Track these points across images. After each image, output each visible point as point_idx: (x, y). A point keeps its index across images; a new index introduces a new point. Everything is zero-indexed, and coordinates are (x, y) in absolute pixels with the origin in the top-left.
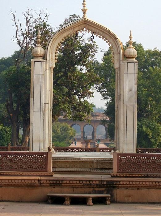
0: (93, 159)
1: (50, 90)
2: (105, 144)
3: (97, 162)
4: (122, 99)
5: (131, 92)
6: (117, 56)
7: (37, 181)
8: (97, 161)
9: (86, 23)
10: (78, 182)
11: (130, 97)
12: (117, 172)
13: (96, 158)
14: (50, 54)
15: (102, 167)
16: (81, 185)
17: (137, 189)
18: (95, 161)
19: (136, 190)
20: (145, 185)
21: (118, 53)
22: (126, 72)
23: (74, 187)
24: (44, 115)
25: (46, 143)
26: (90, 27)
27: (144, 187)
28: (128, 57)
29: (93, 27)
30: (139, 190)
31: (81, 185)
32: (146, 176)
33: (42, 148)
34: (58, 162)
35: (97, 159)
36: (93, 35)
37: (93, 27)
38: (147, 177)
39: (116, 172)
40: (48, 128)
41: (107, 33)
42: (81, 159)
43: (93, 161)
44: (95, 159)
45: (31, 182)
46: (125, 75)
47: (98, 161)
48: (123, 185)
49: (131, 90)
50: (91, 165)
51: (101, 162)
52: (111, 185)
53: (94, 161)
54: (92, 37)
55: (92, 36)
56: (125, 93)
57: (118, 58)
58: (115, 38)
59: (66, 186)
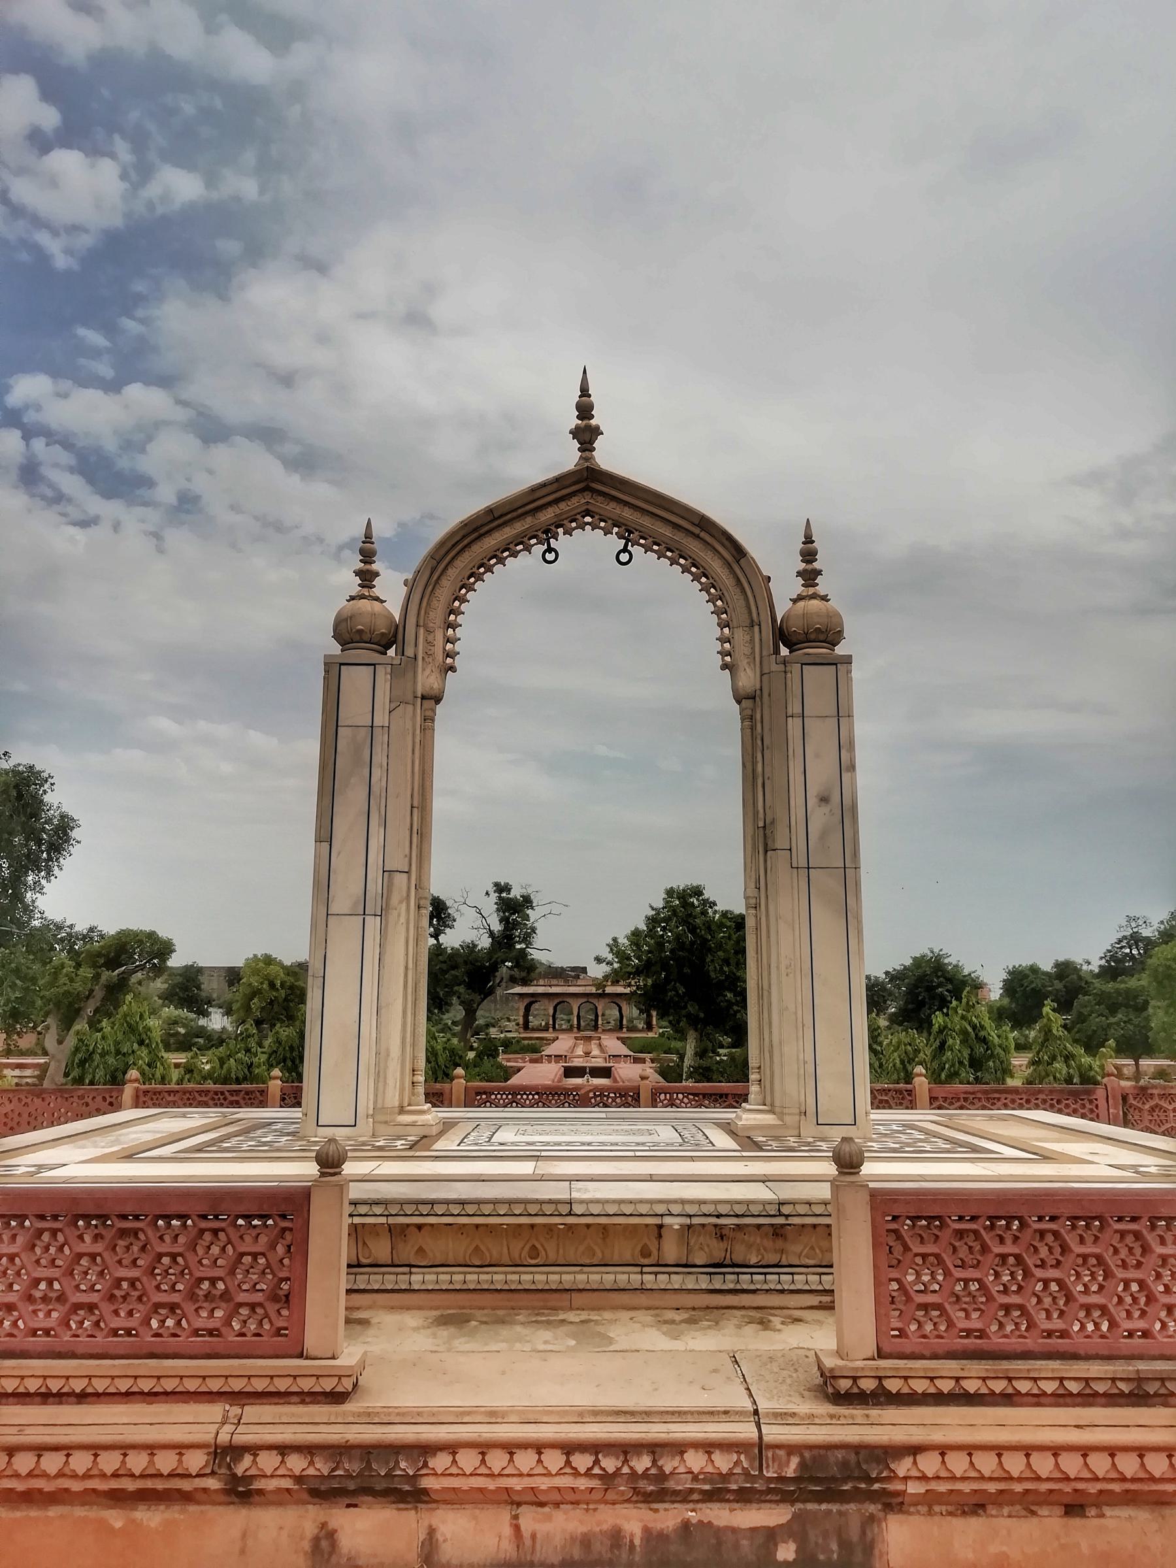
0: (660, 1209)
1: (415, 804)
2: (623, 1041)
3: (690, 1226)
4: (781, 842)
5: (825, 809)
6: (748, 638)
7: (196, 1461)
8: (687, 1221)
9: (594, 485)
10: (554, 1460)
11: (824, 835)
12: (881, 1355)
13: (683, 1202)
14: (422, 630)
15: (718, 1256)
16: (583, 1483)
17: (1060, 1510)
18: (675, 1222)
19: (1051, 1521)
20: (1134, 1480)
21: (752, 621)
22: (797, 709)
23: (519, 1504)
24: (383, 932)
25: (390, 1081)
26: (613, 505)
27: (1130, 1499)
28: (802, 637)
29: (626, 504)
30: (1076, 1522)
31: (583, 1483)
32: (1124, 1387)
33: (371, 1112)
34: (420, 1227)
35: (691, 1209)
36: (629, 548)
37: (626, 504)
38: (1138, 1396)
39: (872, 1350)
40: (400, 1001)
41: (697, 530)
42: (578, 1209)
43: (657, 1221)
44: (675, 1209)
45: (151, 1463)
46: (794, 725)
47: (696, 1221)
48: (942, 1487)
49: (824, 799)
50: (645, 1247)
51: (716, 1226)
52: (845, 1480)
53: (667, 1220)
54: (624, 557)
55: (625, 550)
56: (798, 813)
57: (753, 648)
58: (739, 552)
59: (452, 1496)
